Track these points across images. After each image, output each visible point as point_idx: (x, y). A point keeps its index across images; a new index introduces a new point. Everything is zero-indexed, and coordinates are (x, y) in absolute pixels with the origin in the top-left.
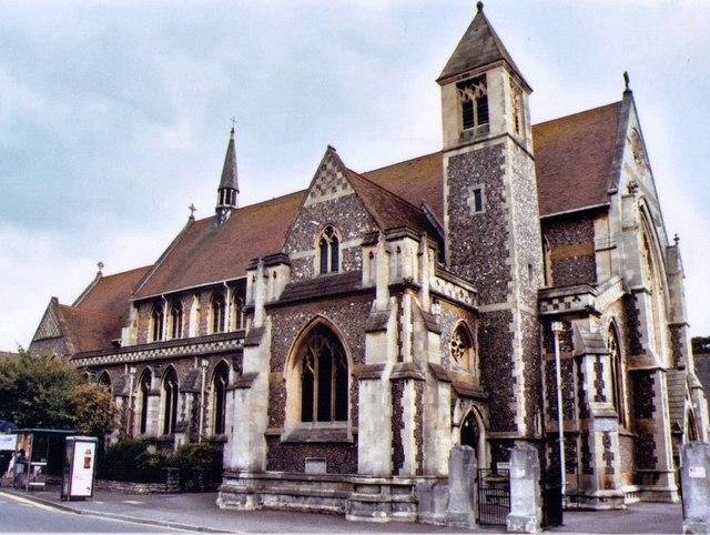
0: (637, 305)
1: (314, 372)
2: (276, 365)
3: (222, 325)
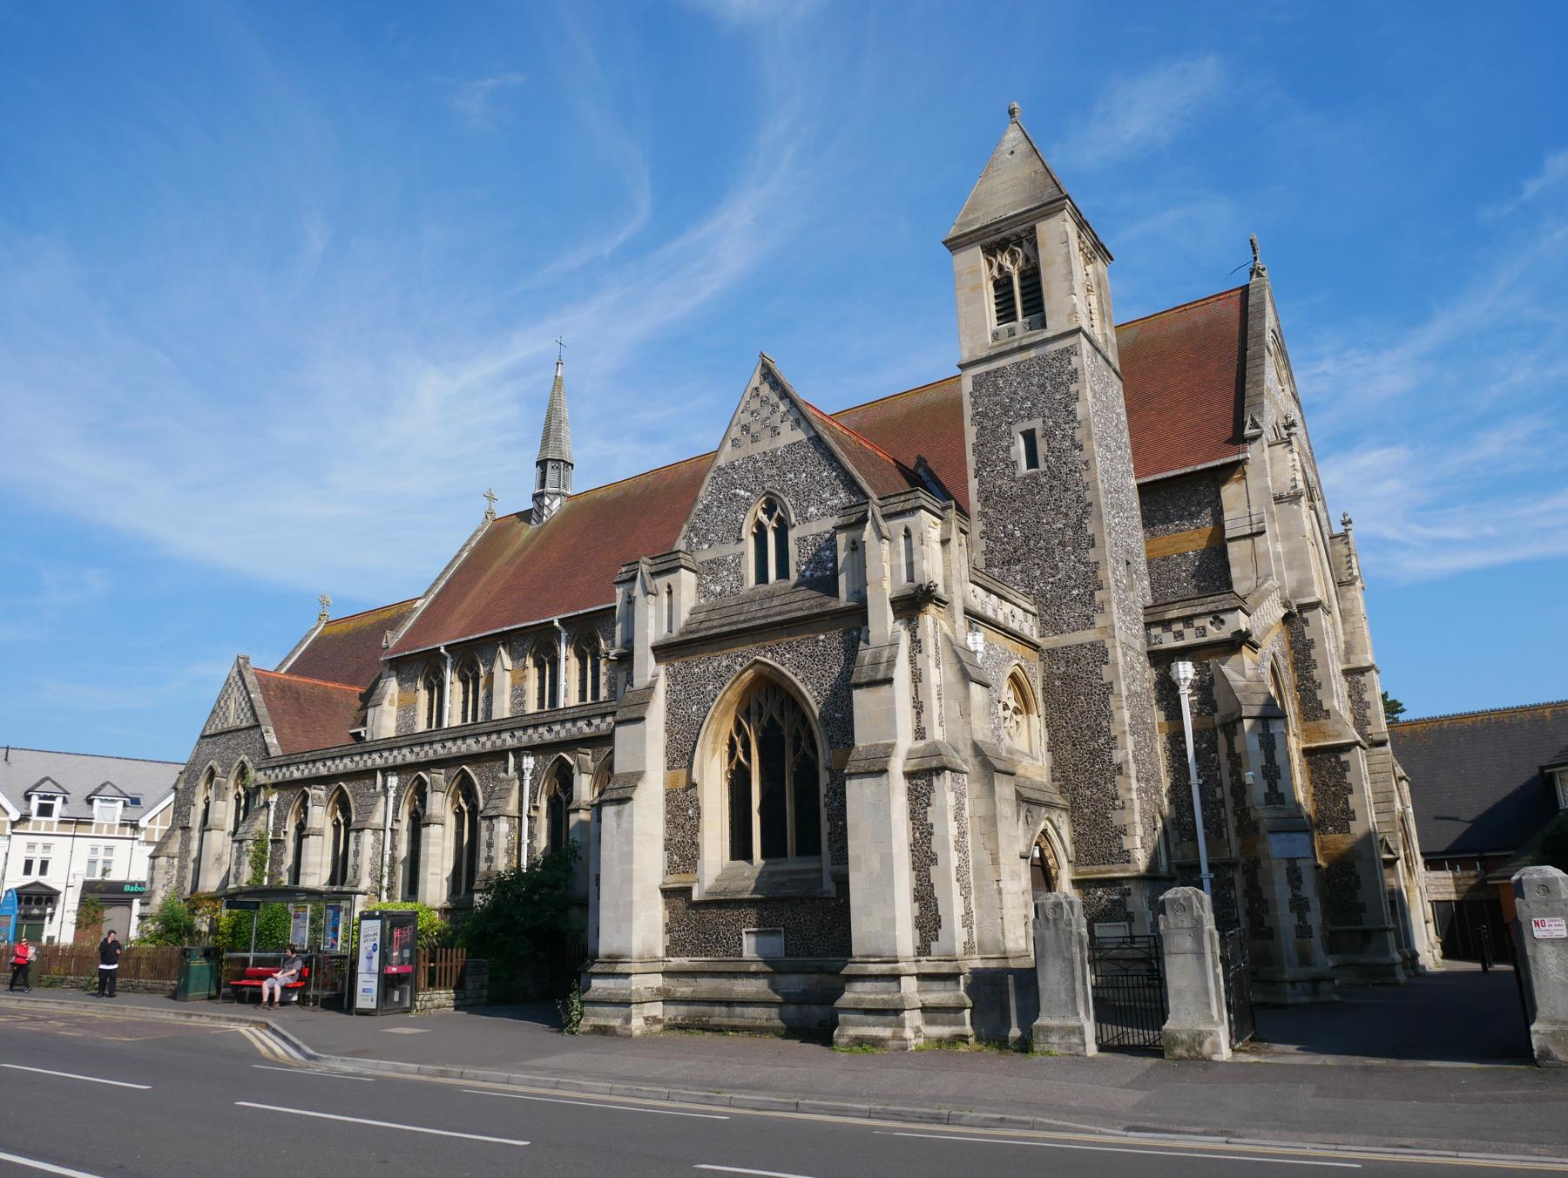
0: (1309, 633)
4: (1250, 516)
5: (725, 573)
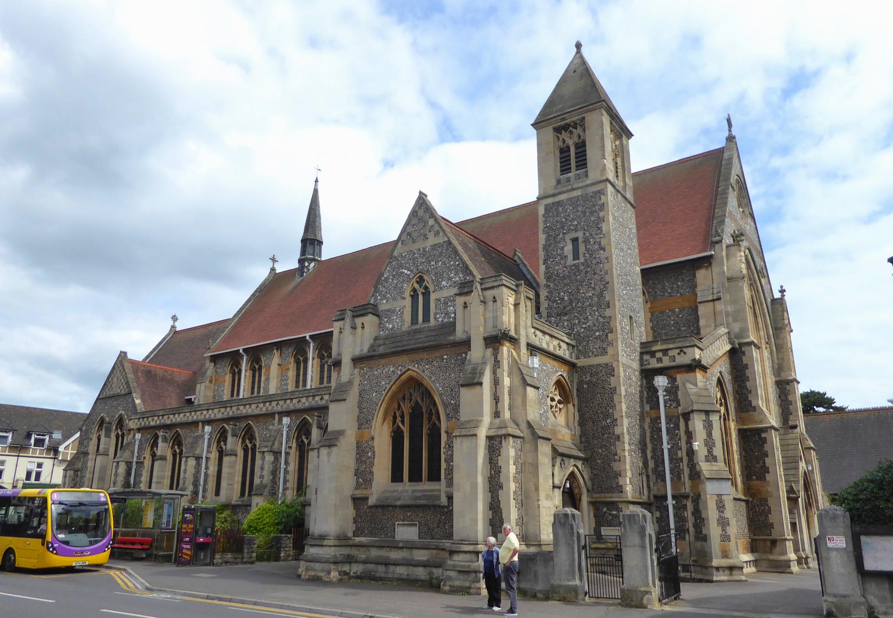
0: (745, 360)
1: (406, 429)
2: (364, 422)
3: (305, 381)
4: (713, 288)
5: (395, 318)
